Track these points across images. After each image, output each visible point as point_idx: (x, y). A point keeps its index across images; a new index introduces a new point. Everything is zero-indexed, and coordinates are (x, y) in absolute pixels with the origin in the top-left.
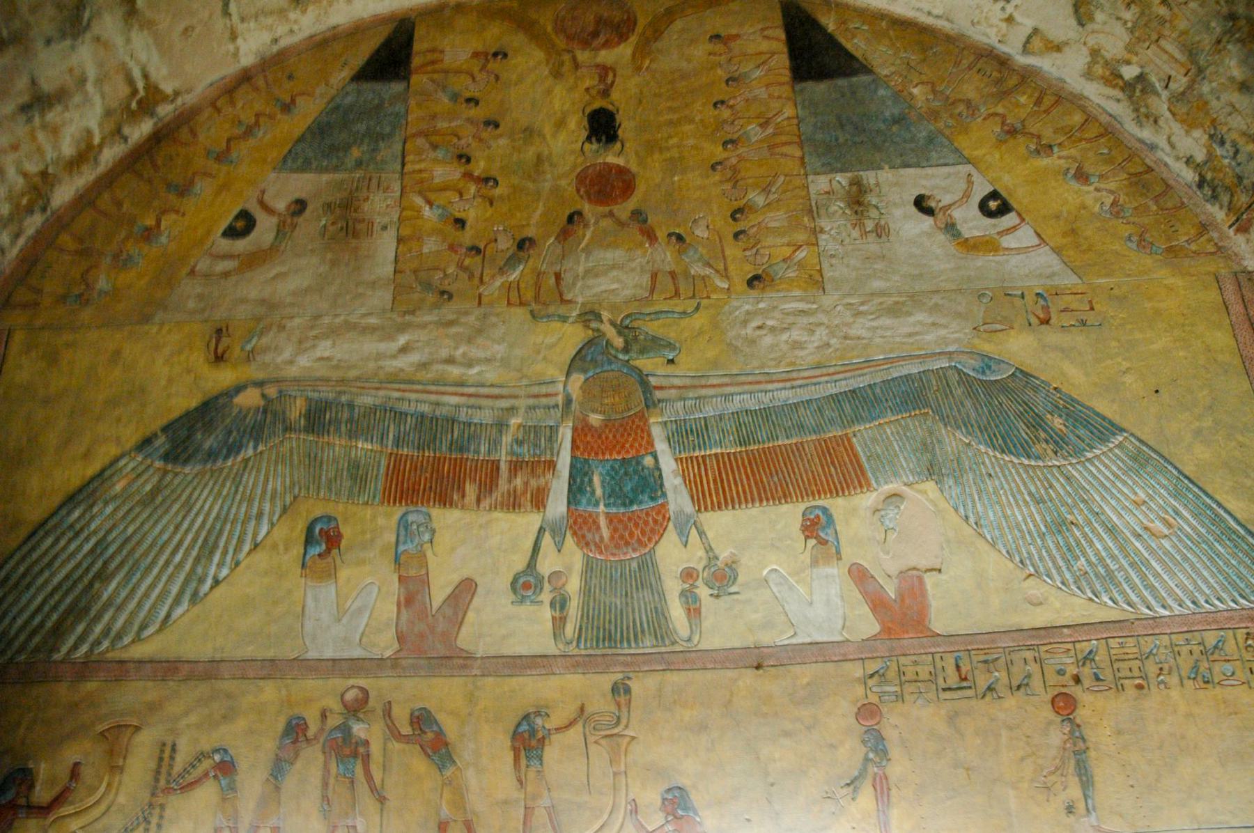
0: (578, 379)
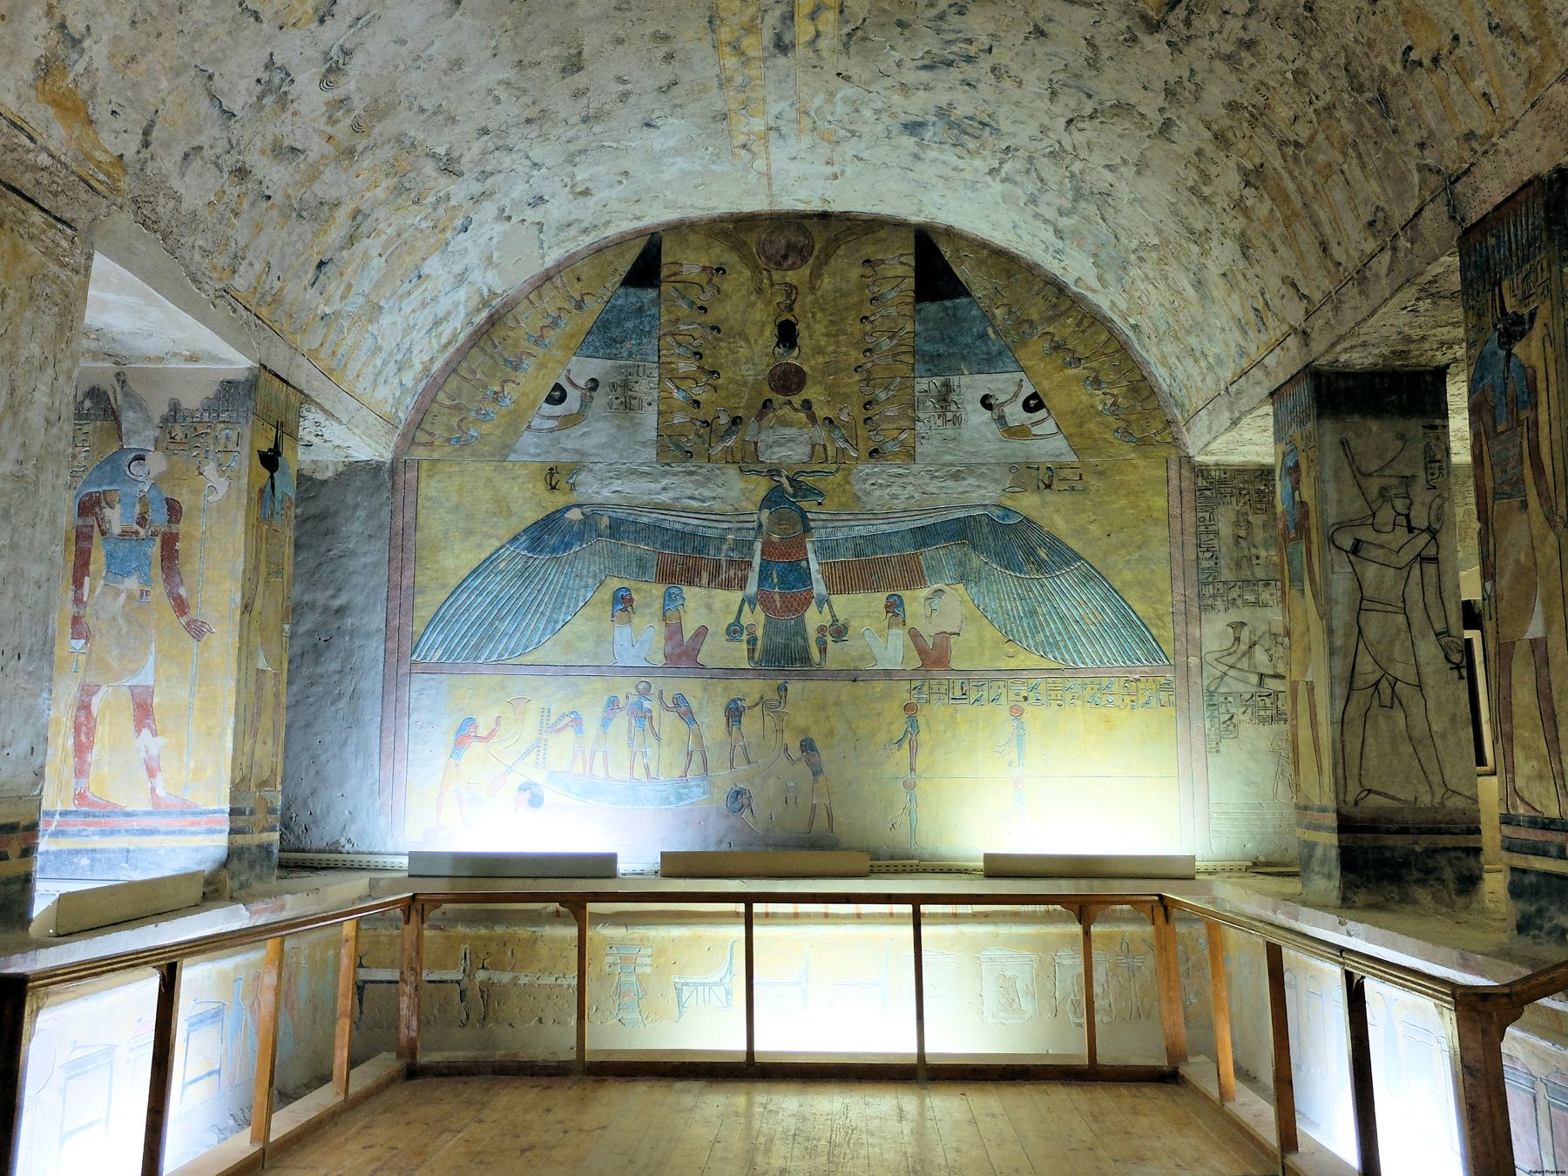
0: (766, 513)
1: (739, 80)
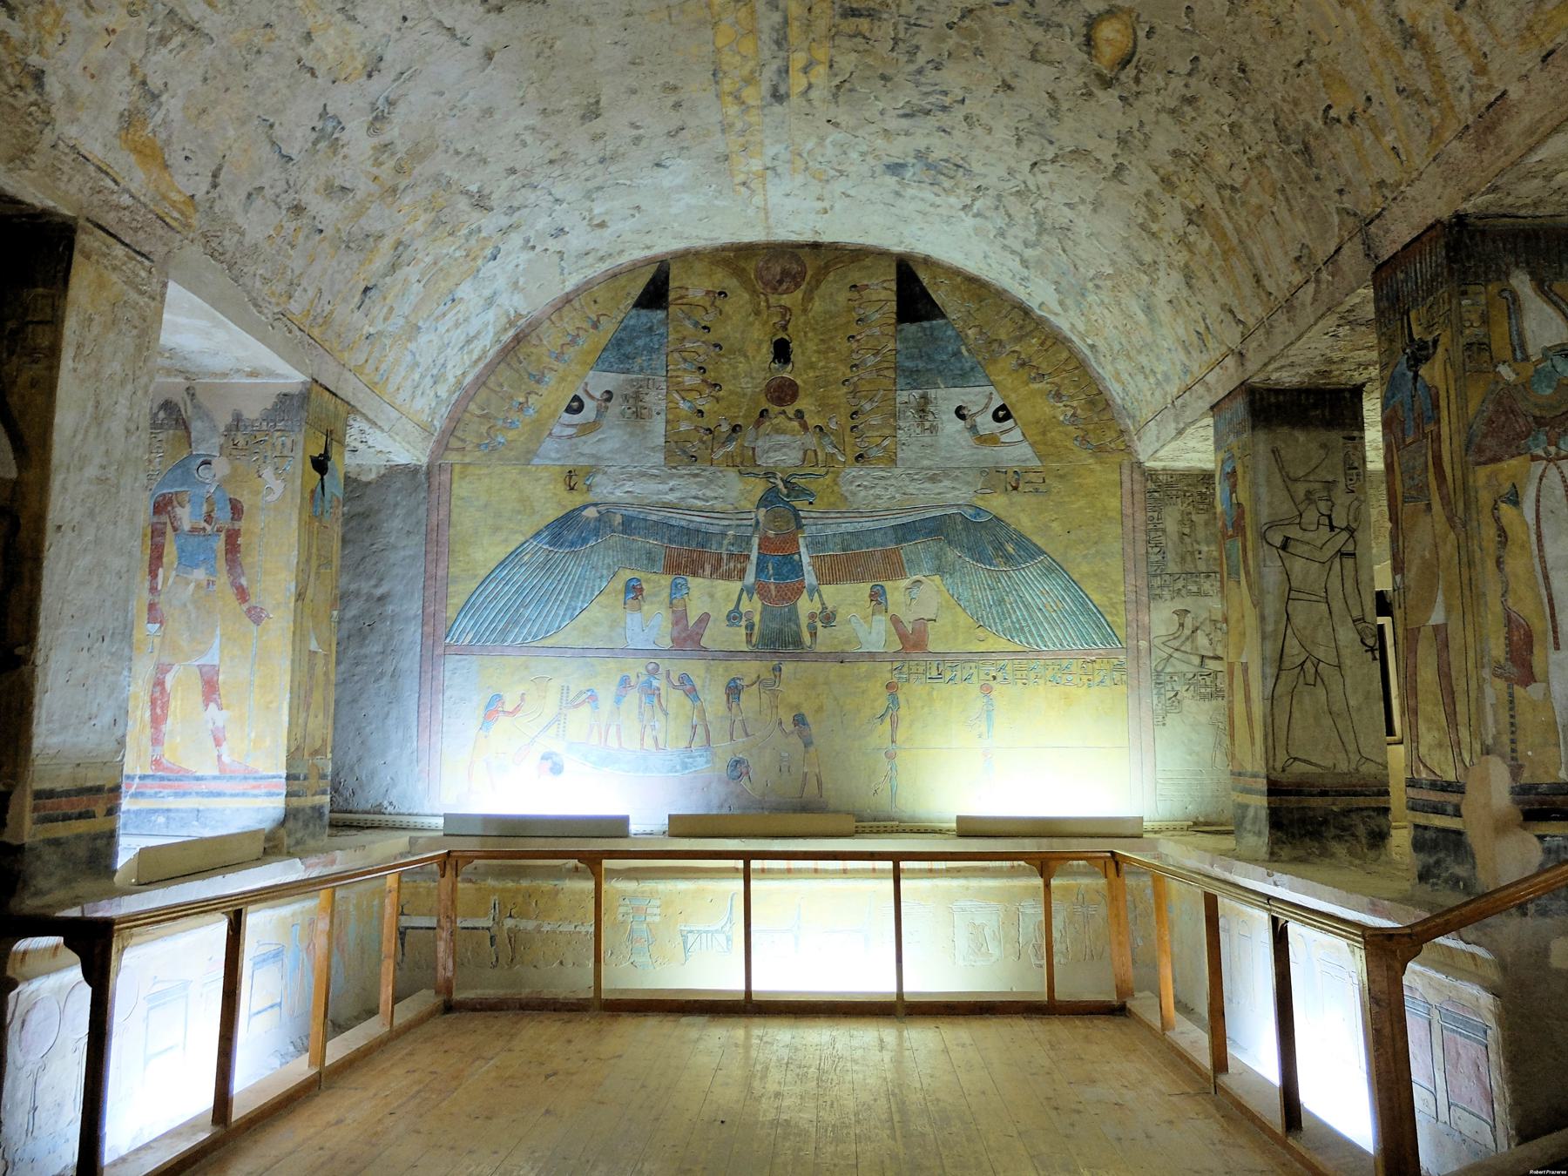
0: (762, 511)
1: (739, 125)
